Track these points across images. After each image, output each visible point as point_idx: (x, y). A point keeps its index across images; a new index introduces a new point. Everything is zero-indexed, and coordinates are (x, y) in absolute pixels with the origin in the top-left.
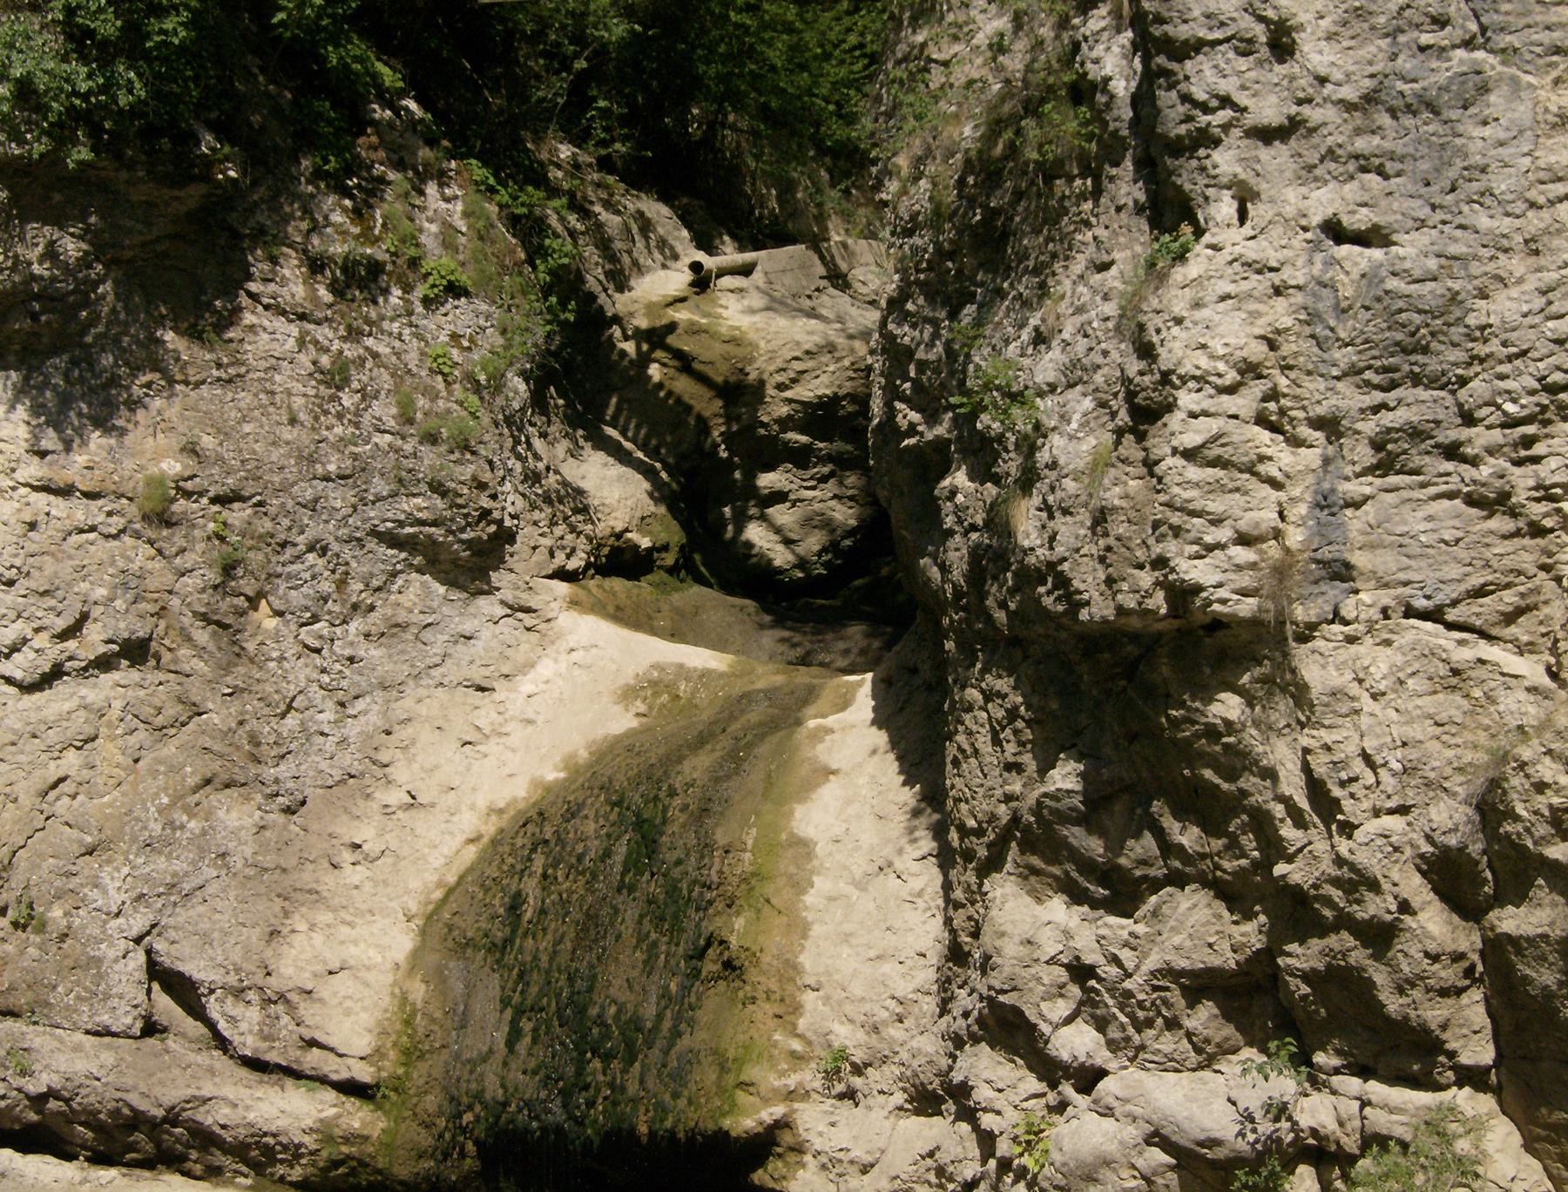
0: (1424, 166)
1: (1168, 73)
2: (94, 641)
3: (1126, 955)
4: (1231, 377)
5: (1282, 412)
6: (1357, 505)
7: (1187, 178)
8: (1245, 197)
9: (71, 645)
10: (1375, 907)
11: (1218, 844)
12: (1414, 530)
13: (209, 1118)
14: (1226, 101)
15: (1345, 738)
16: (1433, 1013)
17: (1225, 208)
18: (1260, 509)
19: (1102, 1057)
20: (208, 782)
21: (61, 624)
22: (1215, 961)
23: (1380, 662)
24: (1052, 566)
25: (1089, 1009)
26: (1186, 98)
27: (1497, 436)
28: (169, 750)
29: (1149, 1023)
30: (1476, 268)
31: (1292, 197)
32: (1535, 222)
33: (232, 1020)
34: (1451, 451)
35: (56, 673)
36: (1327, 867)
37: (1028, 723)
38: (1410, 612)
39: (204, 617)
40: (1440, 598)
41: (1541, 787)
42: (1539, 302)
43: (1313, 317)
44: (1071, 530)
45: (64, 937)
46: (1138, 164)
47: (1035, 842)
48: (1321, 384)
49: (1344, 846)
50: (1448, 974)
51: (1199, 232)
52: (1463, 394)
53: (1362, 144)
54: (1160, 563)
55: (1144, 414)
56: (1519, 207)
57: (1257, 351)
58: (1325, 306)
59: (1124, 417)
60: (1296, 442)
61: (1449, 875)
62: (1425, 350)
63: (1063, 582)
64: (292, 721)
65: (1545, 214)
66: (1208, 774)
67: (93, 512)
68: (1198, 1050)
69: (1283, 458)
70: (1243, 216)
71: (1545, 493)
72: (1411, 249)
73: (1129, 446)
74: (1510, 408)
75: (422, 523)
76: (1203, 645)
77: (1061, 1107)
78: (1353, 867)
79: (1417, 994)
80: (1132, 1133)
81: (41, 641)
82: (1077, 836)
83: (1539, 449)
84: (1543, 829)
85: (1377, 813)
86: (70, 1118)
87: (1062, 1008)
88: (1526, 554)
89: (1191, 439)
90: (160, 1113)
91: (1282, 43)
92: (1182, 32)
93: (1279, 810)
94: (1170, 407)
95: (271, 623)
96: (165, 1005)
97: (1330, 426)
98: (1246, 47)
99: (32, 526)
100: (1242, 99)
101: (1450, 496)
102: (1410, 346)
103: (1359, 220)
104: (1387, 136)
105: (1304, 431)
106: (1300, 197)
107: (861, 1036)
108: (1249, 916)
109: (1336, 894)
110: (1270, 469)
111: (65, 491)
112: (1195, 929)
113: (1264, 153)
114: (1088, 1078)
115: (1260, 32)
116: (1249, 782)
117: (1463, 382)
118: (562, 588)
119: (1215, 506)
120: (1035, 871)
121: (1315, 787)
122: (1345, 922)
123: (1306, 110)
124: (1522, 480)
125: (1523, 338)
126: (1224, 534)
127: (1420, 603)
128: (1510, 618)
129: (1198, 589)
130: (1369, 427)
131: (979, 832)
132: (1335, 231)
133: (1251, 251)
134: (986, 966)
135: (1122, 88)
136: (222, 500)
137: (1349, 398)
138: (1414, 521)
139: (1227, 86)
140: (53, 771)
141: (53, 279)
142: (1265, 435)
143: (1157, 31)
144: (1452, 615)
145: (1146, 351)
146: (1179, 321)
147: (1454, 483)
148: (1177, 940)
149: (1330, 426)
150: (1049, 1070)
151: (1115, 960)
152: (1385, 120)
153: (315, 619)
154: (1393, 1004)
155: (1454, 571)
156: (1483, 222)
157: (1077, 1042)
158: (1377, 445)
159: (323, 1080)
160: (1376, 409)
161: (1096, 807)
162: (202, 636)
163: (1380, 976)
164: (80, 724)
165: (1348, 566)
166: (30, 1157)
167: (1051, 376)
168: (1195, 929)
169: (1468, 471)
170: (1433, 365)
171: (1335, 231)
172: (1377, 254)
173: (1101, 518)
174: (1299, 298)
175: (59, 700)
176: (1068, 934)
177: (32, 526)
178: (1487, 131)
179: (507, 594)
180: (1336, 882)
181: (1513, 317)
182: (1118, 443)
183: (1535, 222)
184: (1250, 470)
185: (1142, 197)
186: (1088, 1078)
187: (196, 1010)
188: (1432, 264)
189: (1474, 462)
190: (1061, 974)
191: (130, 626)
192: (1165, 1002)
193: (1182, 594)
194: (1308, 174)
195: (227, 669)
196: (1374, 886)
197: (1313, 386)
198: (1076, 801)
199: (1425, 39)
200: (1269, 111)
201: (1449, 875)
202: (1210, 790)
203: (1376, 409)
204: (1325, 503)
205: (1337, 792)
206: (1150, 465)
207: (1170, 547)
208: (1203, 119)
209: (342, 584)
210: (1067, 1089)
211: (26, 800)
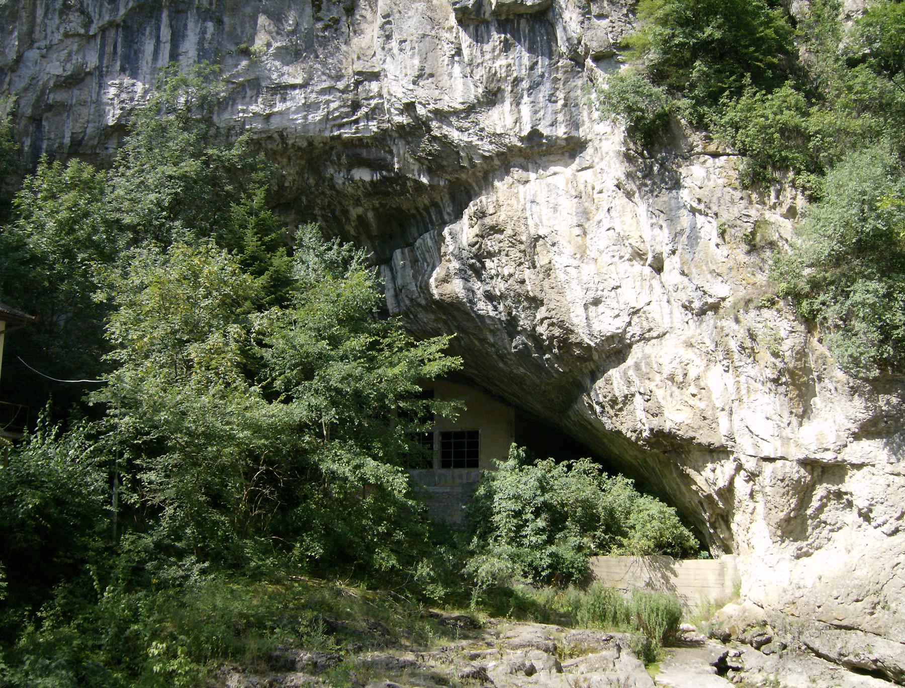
9: (901, 522)
45: (895, 613)
81: (892, 520)
99: (889, 486)
111: (898, 474)
140: (896, 561)
141: (889, 411)
166: (878, 680)
177: (889, 486)
211: (888, 569)
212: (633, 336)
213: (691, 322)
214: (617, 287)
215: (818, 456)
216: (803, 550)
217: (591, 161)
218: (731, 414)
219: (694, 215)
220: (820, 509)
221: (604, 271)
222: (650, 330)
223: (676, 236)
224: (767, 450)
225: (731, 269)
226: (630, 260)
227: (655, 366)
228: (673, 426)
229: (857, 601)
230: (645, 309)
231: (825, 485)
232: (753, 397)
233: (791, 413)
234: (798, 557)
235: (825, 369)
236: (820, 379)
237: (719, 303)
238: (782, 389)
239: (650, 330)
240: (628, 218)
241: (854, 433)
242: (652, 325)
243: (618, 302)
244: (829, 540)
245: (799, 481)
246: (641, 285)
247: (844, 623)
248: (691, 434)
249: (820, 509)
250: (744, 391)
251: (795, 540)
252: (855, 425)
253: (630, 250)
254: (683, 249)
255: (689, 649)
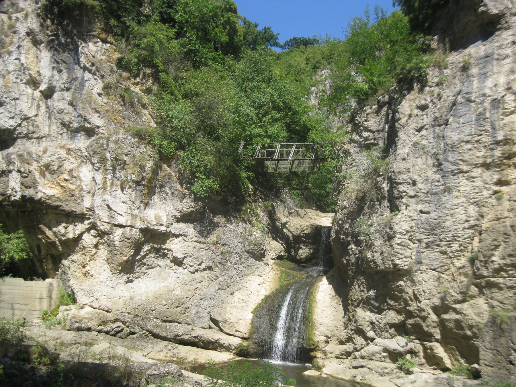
0: (436, 203)
1: (395, 187)
2: (203, 266)
3: (380, 321)
4: (405, 233)
5: (412, 238)
6: (423, 253)
7: (397, 203)
8: (407, 206)
10: (423, 314)
11: (397, 304)
12: (432, 256)
13: (222, 342)
14: (405, 192)
15: (420, 288)
16: (432, 330)
17: (404, 207)
18: (408, 253)
19: (375, 336)
20: (219, 289)
21: (198, 263)
22: (395, 322)
23: (426, 277)
24: (373, 260)
25: (373, 329)
26: (398, 191)
27: (445, 243)
28: (213, 284)
29: (383, 331)
30: (443, 218)
31: (415, 206)
32: (452, 212)
33: (224, 327)
34: (438, 245)
35: (197, 271)
36: (416, 308)
37: (365, 284)
38: (431, 269)
39: (220, 263)
40: (435, 267)
41: (452, 296)
42: (453, 223)
43: (418, 224)
44: (377, 255)
46: (388, 200)
47: (366, 303)
48: (418, 234)
49: (419, 305)
50: (435, 324)
51: (399, 211)
52: (440, 237)
53: (426, 199)
54: (393, 260)
55: (390, 238)
56: (450, 209)
57: (409, 229)
58: (420, 222)
59: (386, 238)
60: (414, 243)
61: (436, 310)
62: (434, 230)
63: (375, 263)
64: (232, 280)
65: (454, 211)
66: (396, 293)
67: (204, 246)
68: (391, 336)
69: (412, 245)
70: (406, 209)
71: (452, 252)
72: (433, 215)
73: (387, 243)
74: (448, 239)
75: (253, 250)
76: (398, 273)
77: (368, 344)
78: (421, 308)
79: (430, 327)
80: (381, 348)
81: (195, 265)
82: (373, 302)
83: (451, 245)
84: (452, 303)
85: (425, 299)
86: (200, 341)
87: (368, 329)
88: (449, 261)
89: (398, 242)
90: (214, 341)
91: (414, 183)
92: (399, 181)
93: (408, 298)
94: (395, 237)
95: (230, 264)
96: (212, 325)
97: (419, 241)
98: (409, 184)
99: (194, 248)
100: (408, 191)
101: (437, 252)
102: (432, 229)
103: (426, 210)
104: (430, 198)
105: (416, 241)
106: (415, 206)
107: (330, 333)
108: (401, 315)
109: (417, 312)
110: (410, 247)
112: (392, 316)
113: (411, 200)
114: (372, 340)
115: (411, 182)
116: (404, 294)
117: (440, 235)
118: (272, 261)
119: (402, 252)
120: (364, 307)
121: (415, 295)
122: (418, 316)
123: (418, 194)
124: (449, 250)
125: (450, 229)
126: (402, 256)
127: (432, 268)
128: (446, 271)
129: (398, 264)
130: (425, 241)
131: (355, 301)
132: (421, 212)
133: (409, 214)
134: (356, 321)
135: (386, 189)
136: (223, 245)
137: (422, 237)
138: (432, 255)
139: (405, 189)
142: (409, 242)
143: (394, 181)
144: (437, 270)
145: (391, 228)
146: (397, 224)
147: (438, 250)
148: (389, 318)
149: (419, 241)
150: (366, 338)
151: (378, 321)
152: (429, 195)
153: (236, 264)
154: (426, 329)
155: (438, 263)
156: (444, 211)
157: (371, 334)
158: (427, 244)
159: (239, 337)
160: (426, 238)
161: (376, 298)
162: (219, 266)
163: (423, 324)
164: (200, 279)
165: (421, 262)
167: (373, 231)
168: (392, 316)
169: (440, 248)
170: (436, 232)
171: (421, 212)
172: (428, 215)
173: (382, 253)
174: (416, 221)
175: (197, 275)
176: (370, 317)
177: (194, 248)
178: (445, 198)
179: (265, 261)
180: (417, 310)
181: (449, 226)
182: (385, 242)
183: (452, 212)
184: (407, 247)
185: (389, 205)
186: (372, 340)
187: (218, 325)
188: (436, 217)
189: (441, 247)
190: (369, 323)
191: (209, 263)
192: (386, 328)
193: (395, 265)
194: (418, 203)
195: (223, 271)
196: (424, 311)
197: (417, 235)
198: (373, 297)
199: (436, 184)
200: (412, 193)
201: (436, 310)
202: (397, 295)
203: (426, 238)
204: (418, 252)
205: (419, 296)
206: (391, 246)
207: (394, 258)
208: (401, 194)
209: (240, 259)
210: (369, 341)
212: (20, 133)
213: (64, 135)
214: (18, 99)
215: (156, 228)
216: (130, 279)
217: (7, 9)
218: (94, 196)
219: (84, 71)
220: (144, 257)
221: (10, 85)
222: (33, 132)
223: (72, 80)
224: (121, 220)
225: (107, 111)
226: (26, 84)
227: (35, 156)
228: (44, 196)
229: (177, 307)
230: (33, 118)
231: (151, 244)
232: (114, 189)
233: (142, 202)
234: (127, 283)
235: (168, 182)
236: (162, 186)
237: (94, 129)
238: (141, 188)
239: (33, 132)
240: (31, 57)
241: (178, 218)
242: (36, 130)
243: (15, 109)
244: (145, 273)
245: (138, 240)
246: (32, 102)
247: (170, 319)
248: (58, 203)
249: (144, 257)
250: (108, 184)
251: (127, 274)
252: (180, 214)
253: (28, 77)
254: (75, 89)
255: (206, 350)
